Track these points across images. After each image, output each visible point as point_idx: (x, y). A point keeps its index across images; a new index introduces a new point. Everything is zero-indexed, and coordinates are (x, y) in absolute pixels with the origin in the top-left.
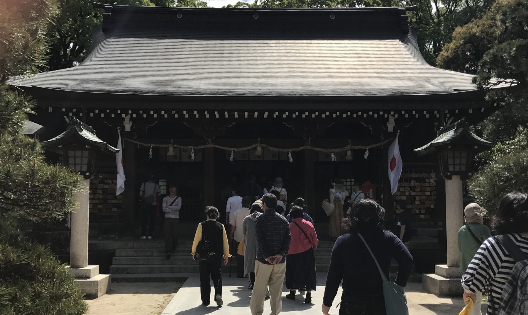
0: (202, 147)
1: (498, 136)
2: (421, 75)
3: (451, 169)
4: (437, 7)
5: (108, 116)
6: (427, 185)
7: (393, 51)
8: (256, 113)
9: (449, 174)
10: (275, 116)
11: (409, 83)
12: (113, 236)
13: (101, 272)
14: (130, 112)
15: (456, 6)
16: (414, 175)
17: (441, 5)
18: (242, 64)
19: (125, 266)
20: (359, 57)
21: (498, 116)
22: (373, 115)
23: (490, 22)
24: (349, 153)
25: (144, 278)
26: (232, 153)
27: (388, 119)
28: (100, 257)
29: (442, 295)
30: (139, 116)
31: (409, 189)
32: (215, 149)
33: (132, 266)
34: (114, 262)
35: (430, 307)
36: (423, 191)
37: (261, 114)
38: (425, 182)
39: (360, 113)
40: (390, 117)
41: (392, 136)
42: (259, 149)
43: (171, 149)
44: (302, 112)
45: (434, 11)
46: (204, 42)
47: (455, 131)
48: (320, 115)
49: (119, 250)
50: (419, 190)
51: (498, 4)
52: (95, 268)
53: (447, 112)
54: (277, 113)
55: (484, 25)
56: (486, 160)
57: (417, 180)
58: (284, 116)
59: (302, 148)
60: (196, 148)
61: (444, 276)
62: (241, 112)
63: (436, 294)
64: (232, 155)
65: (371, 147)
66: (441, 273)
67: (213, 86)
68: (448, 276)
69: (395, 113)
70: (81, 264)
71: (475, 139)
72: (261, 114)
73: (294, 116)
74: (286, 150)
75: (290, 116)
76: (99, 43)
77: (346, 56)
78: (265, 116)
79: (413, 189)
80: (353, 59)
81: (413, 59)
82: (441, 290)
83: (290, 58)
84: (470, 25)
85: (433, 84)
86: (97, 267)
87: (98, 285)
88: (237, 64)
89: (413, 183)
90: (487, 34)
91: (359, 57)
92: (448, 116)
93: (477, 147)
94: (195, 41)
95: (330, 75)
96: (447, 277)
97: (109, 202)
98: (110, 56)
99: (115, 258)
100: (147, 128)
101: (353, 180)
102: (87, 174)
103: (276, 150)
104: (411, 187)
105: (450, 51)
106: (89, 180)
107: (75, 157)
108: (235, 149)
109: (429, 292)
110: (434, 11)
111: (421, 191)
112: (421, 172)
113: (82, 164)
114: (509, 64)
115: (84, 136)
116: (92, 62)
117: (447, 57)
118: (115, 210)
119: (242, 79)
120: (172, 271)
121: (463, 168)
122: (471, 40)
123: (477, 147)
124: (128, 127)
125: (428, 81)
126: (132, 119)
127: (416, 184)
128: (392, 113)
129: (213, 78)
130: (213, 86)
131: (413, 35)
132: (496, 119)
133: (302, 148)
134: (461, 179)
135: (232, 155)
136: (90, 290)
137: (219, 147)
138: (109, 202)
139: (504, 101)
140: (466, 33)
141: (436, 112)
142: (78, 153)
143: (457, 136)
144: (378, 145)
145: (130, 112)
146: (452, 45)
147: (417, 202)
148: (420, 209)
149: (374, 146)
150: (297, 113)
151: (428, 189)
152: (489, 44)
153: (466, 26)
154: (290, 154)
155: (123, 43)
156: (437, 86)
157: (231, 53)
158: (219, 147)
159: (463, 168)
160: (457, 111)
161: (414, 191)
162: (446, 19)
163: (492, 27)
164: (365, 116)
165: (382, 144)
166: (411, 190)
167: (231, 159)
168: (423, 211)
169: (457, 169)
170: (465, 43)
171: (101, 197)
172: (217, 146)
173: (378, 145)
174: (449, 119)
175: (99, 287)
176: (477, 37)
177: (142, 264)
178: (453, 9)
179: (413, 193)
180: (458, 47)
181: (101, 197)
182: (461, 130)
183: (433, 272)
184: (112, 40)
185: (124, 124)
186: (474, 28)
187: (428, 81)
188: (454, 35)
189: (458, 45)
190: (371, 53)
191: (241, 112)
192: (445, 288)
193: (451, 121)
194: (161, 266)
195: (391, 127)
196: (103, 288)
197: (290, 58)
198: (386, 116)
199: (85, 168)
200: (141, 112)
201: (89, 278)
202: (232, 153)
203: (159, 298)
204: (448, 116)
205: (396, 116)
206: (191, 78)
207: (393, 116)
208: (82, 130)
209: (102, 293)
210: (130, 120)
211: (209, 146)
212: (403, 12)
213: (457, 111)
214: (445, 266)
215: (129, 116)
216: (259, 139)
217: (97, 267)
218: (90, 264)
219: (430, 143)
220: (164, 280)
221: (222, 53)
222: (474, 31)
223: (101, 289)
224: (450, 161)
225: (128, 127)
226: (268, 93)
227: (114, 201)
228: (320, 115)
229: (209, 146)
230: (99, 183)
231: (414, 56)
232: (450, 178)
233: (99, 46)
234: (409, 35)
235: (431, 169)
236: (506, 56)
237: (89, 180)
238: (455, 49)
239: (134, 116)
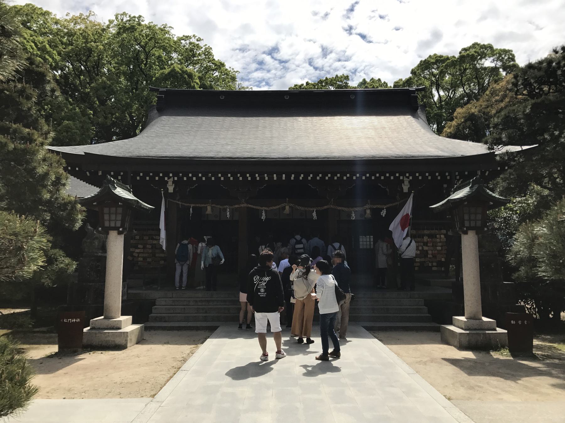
0: (236, 206)
1: (509, 192)
2: (431, 144)
3: (467, 224)
4: (439, 95)
5: (152, 178)
6: (438, 240)
7: (405, 124)
8: (284, 176)
9: (465, 229)
10: (301, 178)
11: (421, 150)
12: (156, 286)
13: (134, 322)
14: (171, 175)
15: (455, 93)
16: (426, 232)
17: (442, 93)
18: (274, 136)
19: (164, 315)
20: (375, 129)
21: (511, 174)
22: (389, 177)
23: (485, 103)
24: (368, 212)
25: (179, 327)
26: (264, 212)
27: (403, 181)
28: (134, 307)
29: (462, 347)
30: (180, 179)
31: (422, 244)
32: (248, 208)
33: (169, 315)
34: (153, 311)
35: (454, 362)
36: (434, 246)
37: (288, 177)
38: (436, 237)
39: (378, 175)
40: (405, 179)
41: (407, 196)
42: (287, 208)
43: (209, 208)
44: (325, 175)
45: (436, 98)
46: (242, 119)
47: (470, 188)
48: (341, 177)
49: (160, 299)
50: (431, 245)
51: (493, 88)
52: (128, 318)
53: (457, 173)
54: (302, 175)
55: (481, 106)
56: (494, 217)
57: (430, 236)
58: (309, 178)
59: (325, 207)
60: (231, 207)
61: (462, 329)
62: (270, 175)
63: (455, 346)
64: (264, 214)
65: (388, 206)
66: (460, 326)
67: (248, 154)
68: (467, 328)
69: (410, 175)
70: (113, 315)
71: (491, 195)
72: (288, 177)
73: (318, 178)
74: (311, 209)
75: (314, 178)
76: (153, 120)
77: (364, 128)
78: (292, 178)
79: (426, 244)
80: (371, 130)
81: (423, 130)
82: (460, 342)
83: (315, 130)
84: (469, 106)
85: (442, 151)
86: (130, 317)
87: (127, 336)
88: (270, 136)
89: (426, 239)
90: (484, 113)
91: (375, 129)
92: (458, 177)
93: (492, 203)
94: (234, 118)
95: (350, 144)
96: (465, 330)
97: (157, 255)
98: (161, 130)
99: (156, 307)
100: (188, 190)
101: (372, 237)
102: (121, 229)
103: (303, 209)
104: (424, 242)
105: (452, 128)
106: (123, 236)
107: (110, 214)
108: (266, 208)
109: (448, 343)
110: (436, 98)
111: (433, 246)
112: (433, 229)
113: (116, 220)
114: (521, 124)
115: (117, 193)
116: (145, 135)
117: (450, 133)
118: (162, 262)
119: (273, 147)
120: (205, 319)
121: (479, 224)
122: (471, 118)
123: (492, 203)
124: (171, 189)
125: (438, 148)
126: (174, 182)
127: (429, 240)
128: (407, 175)
129: (249, 147)
130: (248, 154)
131: (422, 111)
132: (510, 176)
133: (325, 207)
134: (476, 234)
135: (264, 214)
136: (119, 341)
137: (252, 206)
138: (157, 255)
139: (515, 161)
140: (466, 113)
141: (447, 174)
142: (113, 210)
143: (473, 193)
144: (394, 204)
145: (171, 175)
146: (454, 123)
147: (429, 256)
148: (432, 262)
149: (391, 205)
150: (320, 175)
151: (440, 244)
152: (486, 121)
153: (465, 107)
154: (315, 212)
155: (173, 119)
156: (447, 152)
157: (265, 127)
158: (252, 206)
159: (479, 224)
160: (466, 173)
161: (427, 246)
162: (447, 104)
163: (487, 107)
164: (382, 178)
165: (398, 203)
166: (424, 245)
167: (263, 217)
168: (435, 264)
169: (473, 224)
170: (466, 121)
171: (150, 251)
172: (250, 206)
173: (394, 204)
174: (458, 180)
175: (128, 339)
176: (476, 116)
177: (179, 313)
178: (452, 96)
179: (426, 248)
180: (459, 125)
181: (150, 251)
182: (476, 187)
183: (451, 323)
184: (164, 118)
185: (168, 186)
186: (473, 108)
187: (438, 148)
188: (455, 114)
189: (459, 122)
190: (386, 126)
191: (270, 175)
192: (465, 341)
193: (460, 182)
194: (196, 315)
195: (406, 188)
196: (133, 338)
197: (315, 130)
198: (401, 178)
199: (119, 224)
200: (181, 175)
201: (120, 328)
202: (264, 212)
203: (186, 348)
204: (458, 177)
205: (411, 178)
206: (229, 147)
207: (408, 177)
208: (116, 188)
209: (132, 344)
210: (173, 183)
211: (242, 205)
212: (413, 92)
213: (466, 173)
214: (463, 318)
215: (172, 179)
216: (287, 199)
217: (129, 318)
218: (122, 315)
219: (447, 200)
220: (197, 329)
221: (257, 127)
222: (473, 111)
223: (131, 340)
224: (466, 217)
225: (171, 189)
226: (295, 158)
227: (162, 255)
228: (341, 177)
229: (242, 205)
230: (149, 239)
231: (424, 128)
232: (466, 233)
233: (153, 123)
234: (419, 111)
235: (453, 221)
236: (520, 115)
237: (123, 236)
238: (457, 126)
239: (176, 179)
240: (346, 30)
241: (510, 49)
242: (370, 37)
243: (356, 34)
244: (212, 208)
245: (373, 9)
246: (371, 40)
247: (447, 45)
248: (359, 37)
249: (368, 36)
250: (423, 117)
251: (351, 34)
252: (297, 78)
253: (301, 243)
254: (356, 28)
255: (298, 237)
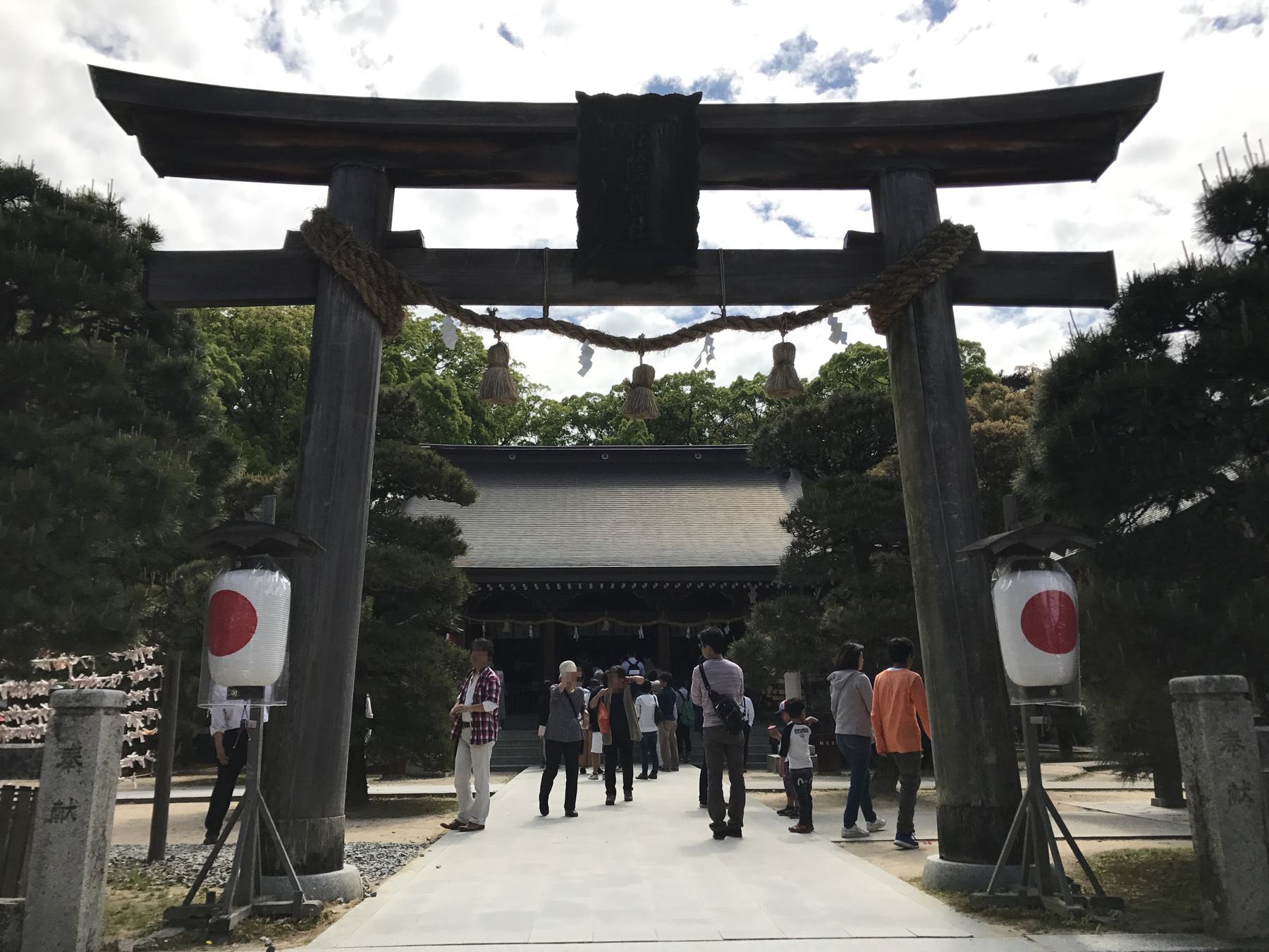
27: (748, 589)
42: (606, 623)
74: (635, 625)
133: (654, 622)
240: (759, 211)
241: (837, 50)
242: (808, 226)
243: (780, 219)
244: (513, 626)
245: (510, 28)
246: (811, 231)
247: (99, 146)
248: (785, 225)
249: (804, 224)
250: (337, 909)
251: (767, 219)
252: (633, 335)
253: (637, 668)
254: (778, 206)
255: (633, 660)
